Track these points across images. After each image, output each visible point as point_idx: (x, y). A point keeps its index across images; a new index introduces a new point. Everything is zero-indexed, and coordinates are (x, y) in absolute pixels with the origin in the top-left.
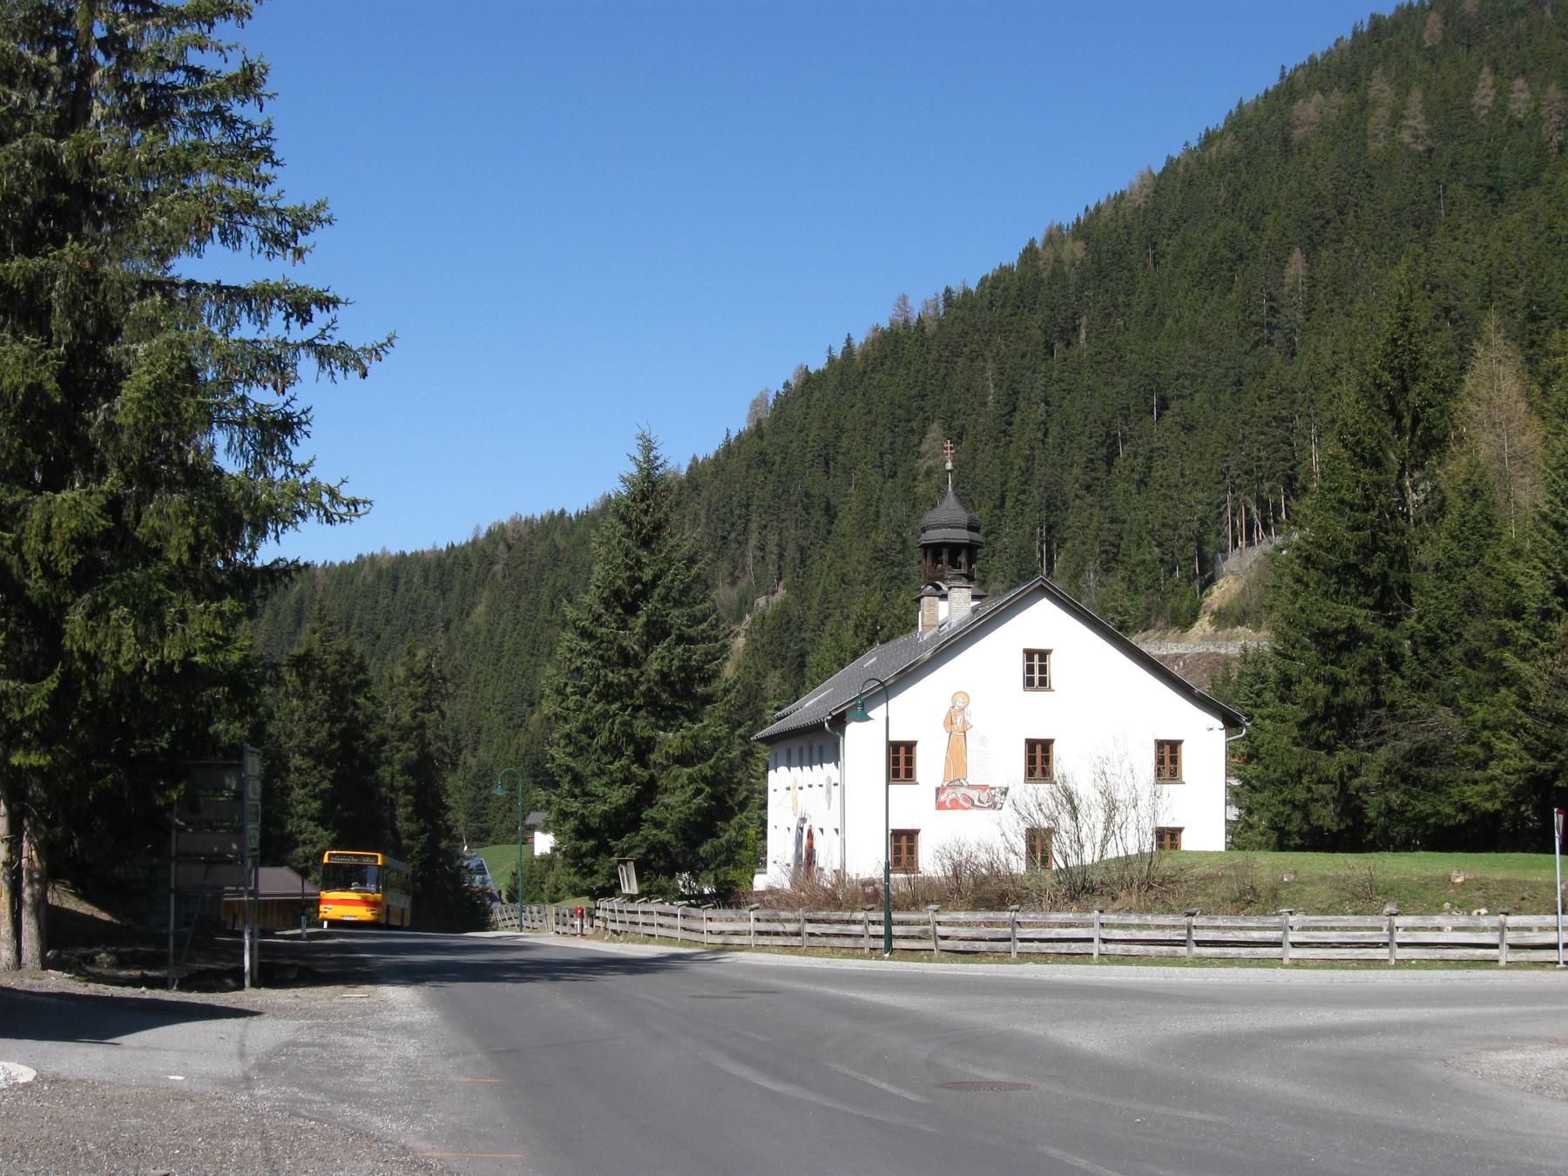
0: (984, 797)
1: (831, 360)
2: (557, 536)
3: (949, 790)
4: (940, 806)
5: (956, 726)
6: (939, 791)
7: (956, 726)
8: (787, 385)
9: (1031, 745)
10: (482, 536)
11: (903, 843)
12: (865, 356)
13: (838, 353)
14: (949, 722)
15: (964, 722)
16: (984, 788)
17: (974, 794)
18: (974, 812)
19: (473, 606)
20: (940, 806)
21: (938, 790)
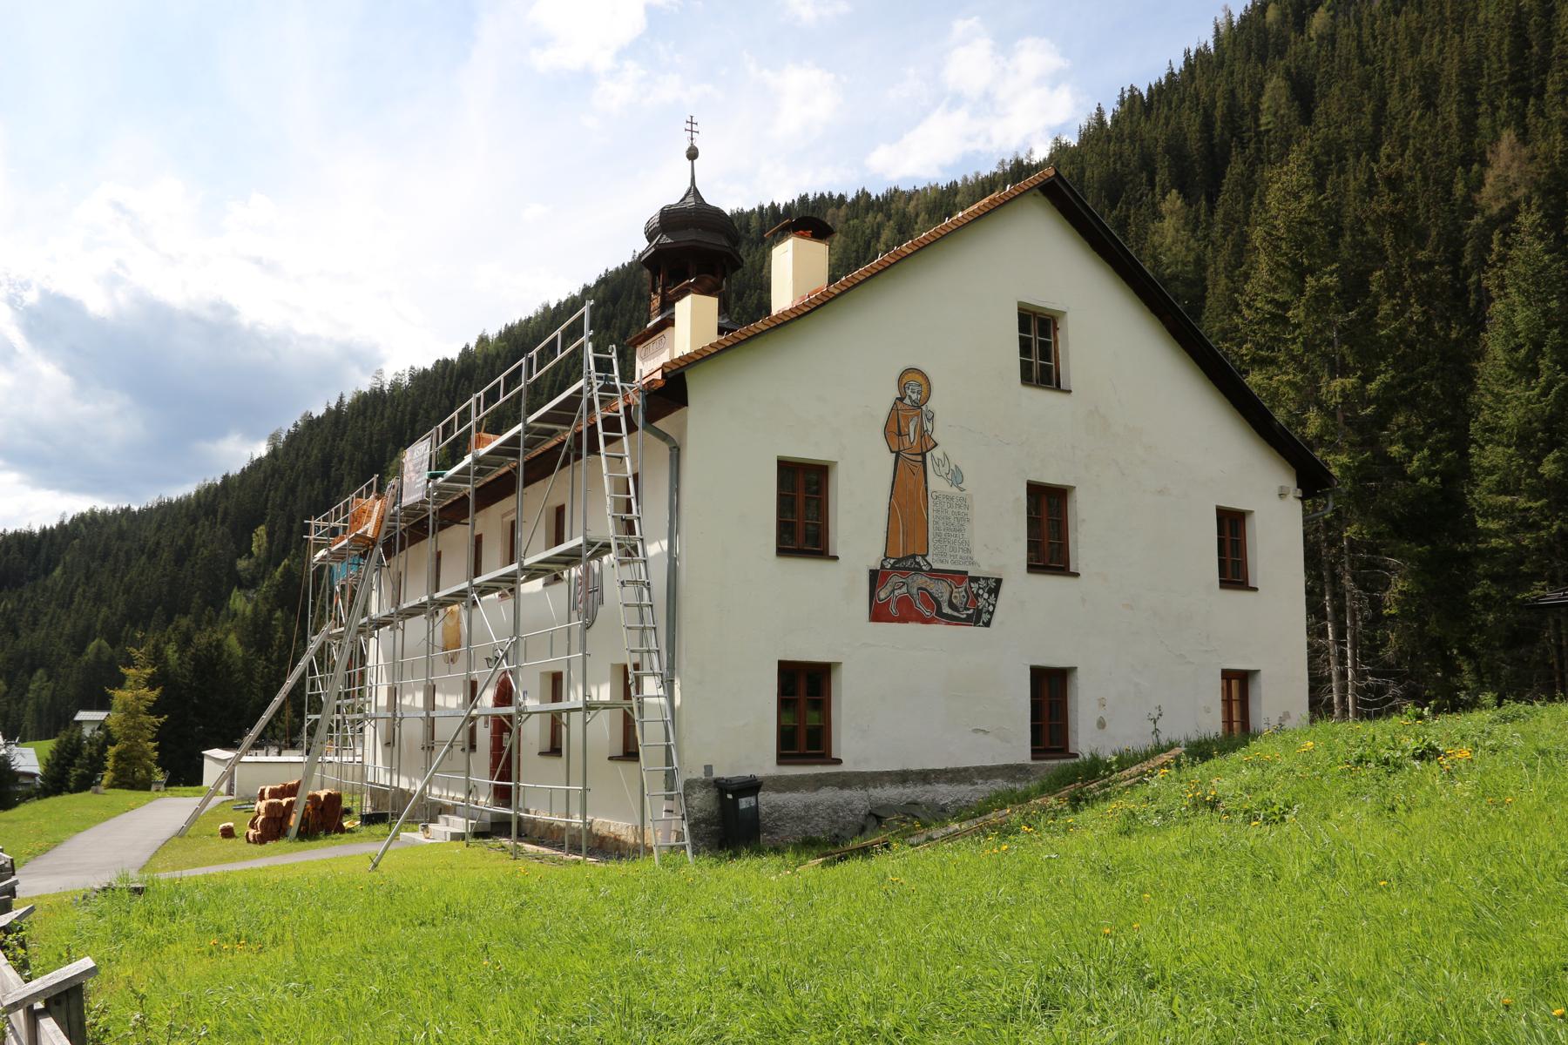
0: (959, 596)
1: (328, 410)
2: (124, 523)
3: (895, 579)
4: (878, 613)
5: (908, 427)
6: (876, 578)
7: (908, 427)
8: (296, 425)
9: (1037, 492)
10: (67, 522)
11: (805, 689)
12: (351, 406)
13: (333, 406)
14: (894, 430)
15: (923, 434)
16: (959, 576)
17: (941, 590)
18: (940, 630)
19: (53, 570)
20: (878, 613)
21: (874, 574)
